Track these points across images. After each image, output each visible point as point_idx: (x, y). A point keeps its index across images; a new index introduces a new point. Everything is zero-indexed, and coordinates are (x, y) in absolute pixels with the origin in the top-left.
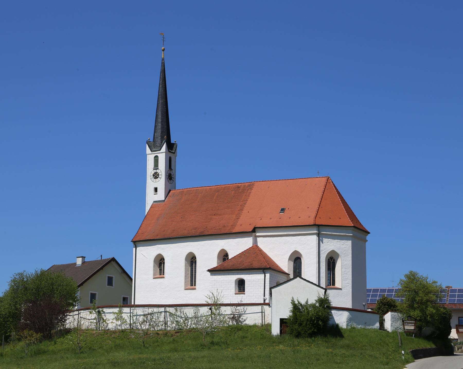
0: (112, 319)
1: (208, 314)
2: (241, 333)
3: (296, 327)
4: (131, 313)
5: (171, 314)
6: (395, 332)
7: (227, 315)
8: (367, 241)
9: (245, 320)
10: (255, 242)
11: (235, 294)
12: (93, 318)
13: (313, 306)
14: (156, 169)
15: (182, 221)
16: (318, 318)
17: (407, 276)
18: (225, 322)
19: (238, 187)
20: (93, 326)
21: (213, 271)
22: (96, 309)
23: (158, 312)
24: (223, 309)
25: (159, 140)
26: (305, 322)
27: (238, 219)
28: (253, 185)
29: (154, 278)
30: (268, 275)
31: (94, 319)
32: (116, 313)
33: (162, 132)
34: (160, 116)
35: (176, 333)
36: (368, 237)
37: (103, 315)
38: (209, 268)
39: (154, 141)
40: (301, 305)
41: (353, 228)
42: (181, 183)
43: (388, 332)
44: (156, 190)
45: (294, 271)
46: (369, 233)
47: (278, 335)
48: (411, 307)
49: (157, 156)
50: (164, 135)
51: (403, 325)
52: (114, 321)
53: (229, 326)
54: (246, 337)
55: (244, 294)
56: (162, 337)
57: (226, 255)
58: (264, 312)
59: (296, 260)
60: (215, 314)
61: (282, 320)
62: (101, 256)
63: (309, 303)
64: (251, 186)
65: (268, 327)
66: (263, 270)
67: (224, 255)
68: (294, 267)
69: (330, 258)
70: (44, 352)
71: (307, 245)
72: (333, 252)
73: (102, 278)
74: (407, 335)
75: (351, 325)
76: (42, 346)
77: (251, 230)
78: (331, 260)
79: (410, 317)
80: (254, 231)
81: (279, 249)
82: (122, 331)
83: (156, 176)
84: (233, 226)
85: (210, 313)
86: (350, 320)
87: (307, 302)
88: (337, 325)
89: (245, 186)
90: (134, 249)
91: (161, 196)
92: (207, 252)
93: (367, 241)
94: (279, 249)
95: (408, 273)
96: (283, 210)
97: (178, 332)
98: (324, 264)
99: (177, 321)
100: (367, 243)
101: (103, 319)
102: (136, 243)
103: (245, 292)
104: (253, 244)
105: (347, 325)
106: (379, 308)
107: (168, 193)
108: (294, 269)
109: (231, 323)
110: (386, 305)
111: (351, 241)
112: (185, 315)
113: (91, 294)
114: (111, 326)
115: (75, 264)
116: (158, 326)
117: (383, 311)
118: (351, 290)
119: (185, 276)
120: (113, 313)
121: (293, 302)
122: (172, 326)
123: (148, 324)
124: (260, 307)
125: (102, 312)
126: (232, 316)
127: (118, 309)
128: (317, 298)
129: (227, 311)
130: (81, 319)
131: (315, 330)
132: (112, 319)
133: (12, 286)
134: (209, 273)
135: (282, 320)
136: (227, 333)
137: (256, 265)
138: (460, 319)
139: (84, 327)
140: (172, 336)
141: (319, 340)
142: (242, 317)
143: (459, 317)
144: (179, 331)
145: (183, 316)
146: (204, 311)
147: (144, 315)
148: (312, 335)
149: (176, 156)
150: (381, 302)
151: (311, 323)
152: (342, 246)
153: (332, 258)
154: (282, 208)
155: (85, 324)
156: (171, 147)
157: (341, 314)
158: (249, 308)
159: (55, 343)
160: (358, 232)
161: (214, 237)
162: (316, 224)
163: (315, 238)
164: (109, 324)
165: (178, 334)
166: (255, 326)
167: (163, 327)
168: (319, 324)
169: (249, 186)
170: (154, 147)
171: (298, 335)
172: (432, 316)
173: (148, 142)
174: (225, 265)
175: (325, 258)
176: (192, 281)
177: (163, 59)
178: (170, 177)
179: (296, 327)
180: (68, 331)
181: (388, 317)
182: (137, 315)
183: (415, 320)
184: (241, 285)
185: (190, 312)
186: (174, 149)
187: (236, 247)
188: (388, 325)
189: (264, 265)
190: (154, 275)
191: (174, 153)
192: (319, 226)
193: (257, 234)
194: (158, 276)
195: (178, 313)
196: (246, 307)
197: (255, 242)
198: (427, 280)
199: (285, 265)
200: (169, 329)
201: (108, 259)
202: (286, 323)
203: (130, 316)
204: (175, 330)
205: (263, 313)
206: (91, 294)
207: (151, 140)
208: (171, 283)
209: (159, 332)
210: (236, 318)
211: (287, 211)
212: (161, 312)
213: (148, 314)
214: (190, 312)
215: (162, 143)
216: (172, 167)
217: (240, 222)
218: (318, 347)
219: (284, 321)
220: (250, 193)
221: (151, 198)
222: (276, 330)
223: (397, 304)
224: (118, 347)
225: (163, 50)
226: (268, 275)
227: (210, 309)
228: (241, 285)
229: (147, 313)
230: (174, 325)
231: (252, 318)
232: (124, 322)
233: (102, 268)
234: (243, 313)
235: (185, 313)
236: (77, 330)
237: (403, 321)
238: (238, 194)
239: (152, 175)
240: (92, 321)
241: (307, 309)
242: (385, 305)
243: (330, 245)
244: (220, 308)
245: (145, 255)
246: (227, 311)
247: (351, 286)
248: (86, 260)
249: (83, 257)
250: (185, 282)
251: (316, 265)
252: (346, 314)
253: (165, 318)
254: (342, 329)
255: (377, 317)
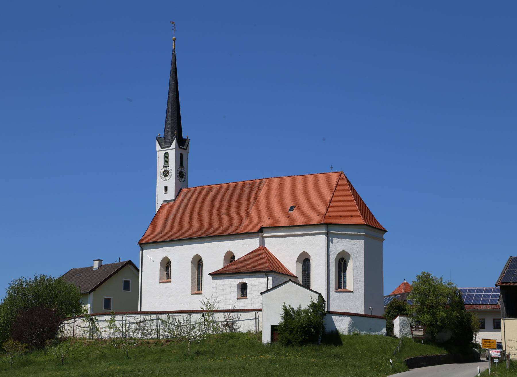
0: (106, 327)
1: (200, 321)
2: (230, 342)
3: (286, 334)
4: (123, 321)
5: (163, 322)
6: (404, 338)
7: (220, 322)
8: (384, 240)
9: (239, 328)
10: (262, 243)
11: (238, 299)
12: (87, 326)
13: (306, 312)
14: (166, 167)
15: (192, 220)
16: (310, 325)
17: (418, 277)
18: (219, 329)
19: (250, 184)
20: (87, 335)
21: (215, 275)
22: (89, 317)
23: (151, 320)
24: (216, 315)
25: (169, 136)
26: (295, 330)
27: (246, 218)
28: (264, 181)
29: (160, 283)
30: (271, 279)
31: (88, 327)
32: (109, 321)
33: (172, 127)
34: (170, 111)
35: (167, 341)
36: (385, 236)
37: (96, 323)
38: (211, 272)
39: (164, 138)
40: (293, 311)
41: (365, 227)
42: (194, 180)
43: (397, 338)
44: (166, 188)
45: (303, 273)
46: (386, 231)
47: (268, 343)
48: (420, 311)
49: (167, 153)
50: (175, 132)
51: (411, 330)
52: (107, 329)
53: (223, 334)
54: (235, 346)
55: (247, 299)
56: (152, 346)
57: (233, 257)
58: (259, 319)
59: (305, 261)
60: (208, 321)
61: (273, 327)
62: (120, 259)
63: (302, 309)
64: (262, 183)
65: (259, 335)
66: (266, 273)
67: (230, 257)
68: (303, 269)
69: (341, 259)
70: (30, 363)
71: (315, 245)
72: (343, 252)
73: (118, 282)
74: (416, 341)
75: (354, 331)
76: (32, 357)
77: (257, 230)
78: (342, 261)
79: (418, 322)
80: (261, 231)
81: (285, 250)
82: (113, 340)
83: (166, 174)
84: (240, 226)
85: (202, 320)
86: (352, 326)
87: (299, 308)
88: (337, 332)
89: (256, 183)
90: (141, 252)
91: (171, 195)
92: (213, 254)
93: (384, 240)
94: (285, 250)
95: (420, 274)
96: (292, 208)
97: (169, 341)
98: (334, 266)
99: (169, 329)
100: (384, 242)
101: (96, 328)
102: (143, 245)
103: (248, 297)
104: (260, 245)
105: (349, 331)
106: (389, 313)
107: (178, 192)
108: (303, 271)
109: (224, 331)
110: (397, 308)
111: (363, 241)
112: (178, 322)
113: (105, 299)
114: (104, 335)
115: (92, 267)
116: (151, 334)
117: (392, 315)
118: (363, 292)
119: (192, 280)
120: (106, 321)
121: (285, 308)
122: (164, 334)
123: (140, 332)
124: (254, 313)
125: (95, 320)
126: (225, 323)
127: (110, 317)
128: (309, 303)
129: (220, 317)
130: (75, 328)
131: (307, 338)
132: (106, 327)
133: (9, 293)
134: (211, 277)
135: (273, 327)
136: (217, 341)
137: (259, 268)
138: (495, 321)
139: (79, 336)
140: (162, 344)
141: (309, 349)
142: (236, 324)
143: (494, 319)
144: (171, 340)
145: (176, 324)
146: (196, 318)
147: (136, 323)
148: (303, 343)
149: (188, 152)
150: (391, 306)
151: (307, 330)
152: (354, 246)
153: (343, 259)
154: (292, 206)
155: (80, 333)
156: (182, 143)
157: (342, 320)
158: (243, 314)
159: (45, 354)
160: (372, 230)
161: (220, 238)
162: (325, 223)
163: (324, 238)
164: (102, 333)
165: (169, 343)
166: (248, 333)
167: (156, 336)
168: (311, 331)
169: (260, 183)
170: (165, 143)
171: (288, 343)
172: (443, 320)
173: (158, 139)
174: (232, 268)
175: (334, 259)
176: (198, 286)
177: (174, 50)
178: (181, 175)
179: (286, 334)
180: (64, 339)
181: (397, 322)
182: (130, 323)
183: (425, 325)
184: (243, 289)
185: (181, 319)
186: (186, 145)
187: (242, 248)
188: (397, 331)
189: (268, 267)
190: (161, 279)
191: (186, 149)
192: (327, 225)
193: (265, 235)
194: (165, 280)
195: (171, 321)
196: (239, 314)
197: (262, 243)
198: (443, 282)
199: (293, 267)
200: (161, 337)
201: (124, 262)
202: (277, 330)
203: (123, 324)
204: (167, 338)
205: (257, 320)
206: (105, 299)
207: (162, 136)
208: (177, 289)
209: (150, 341)
210: (229, 325)
211: (296, 210)
212: (153, 320)
213: (141, 322)
214: (181, 319)
215: (172, 139)
216: (184, 164)
217: (248, 221)
218: (301, 356)
219: (275, 328)
220: (261, 190)
221: (161, 197)
222: (266, 338)
223: (407, 308)
224: (103, 357)
225: (174, 40)
226: (271, 279)
227: (203, 316)
228: (243, 289)
229: (139, 320)
230: (167, 333)
231: (245, 325)
232: (117, 330)
233: (117, 272)
234: (237, 319)
235: (177, 320)
236: (72, 340)
237: (411, 326)
238: (246, 193)
239: (162, 173)
240: (86, 329)
241: (299, 315)
242: (395, 309)
243: (339, 245)
244: (213, 314)
245: (150, 260)
246: (220, 317)
247: (363, 288)
248: (104, 263)
249: (100, 261)
250: (191, 287)
251: (325, 267)
252: (347, 320)
253: (157, 327)
254: (342, 335)
255: (384, 322)
